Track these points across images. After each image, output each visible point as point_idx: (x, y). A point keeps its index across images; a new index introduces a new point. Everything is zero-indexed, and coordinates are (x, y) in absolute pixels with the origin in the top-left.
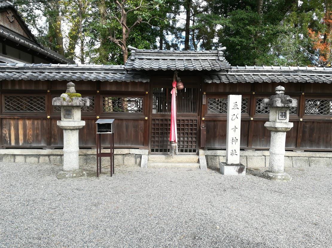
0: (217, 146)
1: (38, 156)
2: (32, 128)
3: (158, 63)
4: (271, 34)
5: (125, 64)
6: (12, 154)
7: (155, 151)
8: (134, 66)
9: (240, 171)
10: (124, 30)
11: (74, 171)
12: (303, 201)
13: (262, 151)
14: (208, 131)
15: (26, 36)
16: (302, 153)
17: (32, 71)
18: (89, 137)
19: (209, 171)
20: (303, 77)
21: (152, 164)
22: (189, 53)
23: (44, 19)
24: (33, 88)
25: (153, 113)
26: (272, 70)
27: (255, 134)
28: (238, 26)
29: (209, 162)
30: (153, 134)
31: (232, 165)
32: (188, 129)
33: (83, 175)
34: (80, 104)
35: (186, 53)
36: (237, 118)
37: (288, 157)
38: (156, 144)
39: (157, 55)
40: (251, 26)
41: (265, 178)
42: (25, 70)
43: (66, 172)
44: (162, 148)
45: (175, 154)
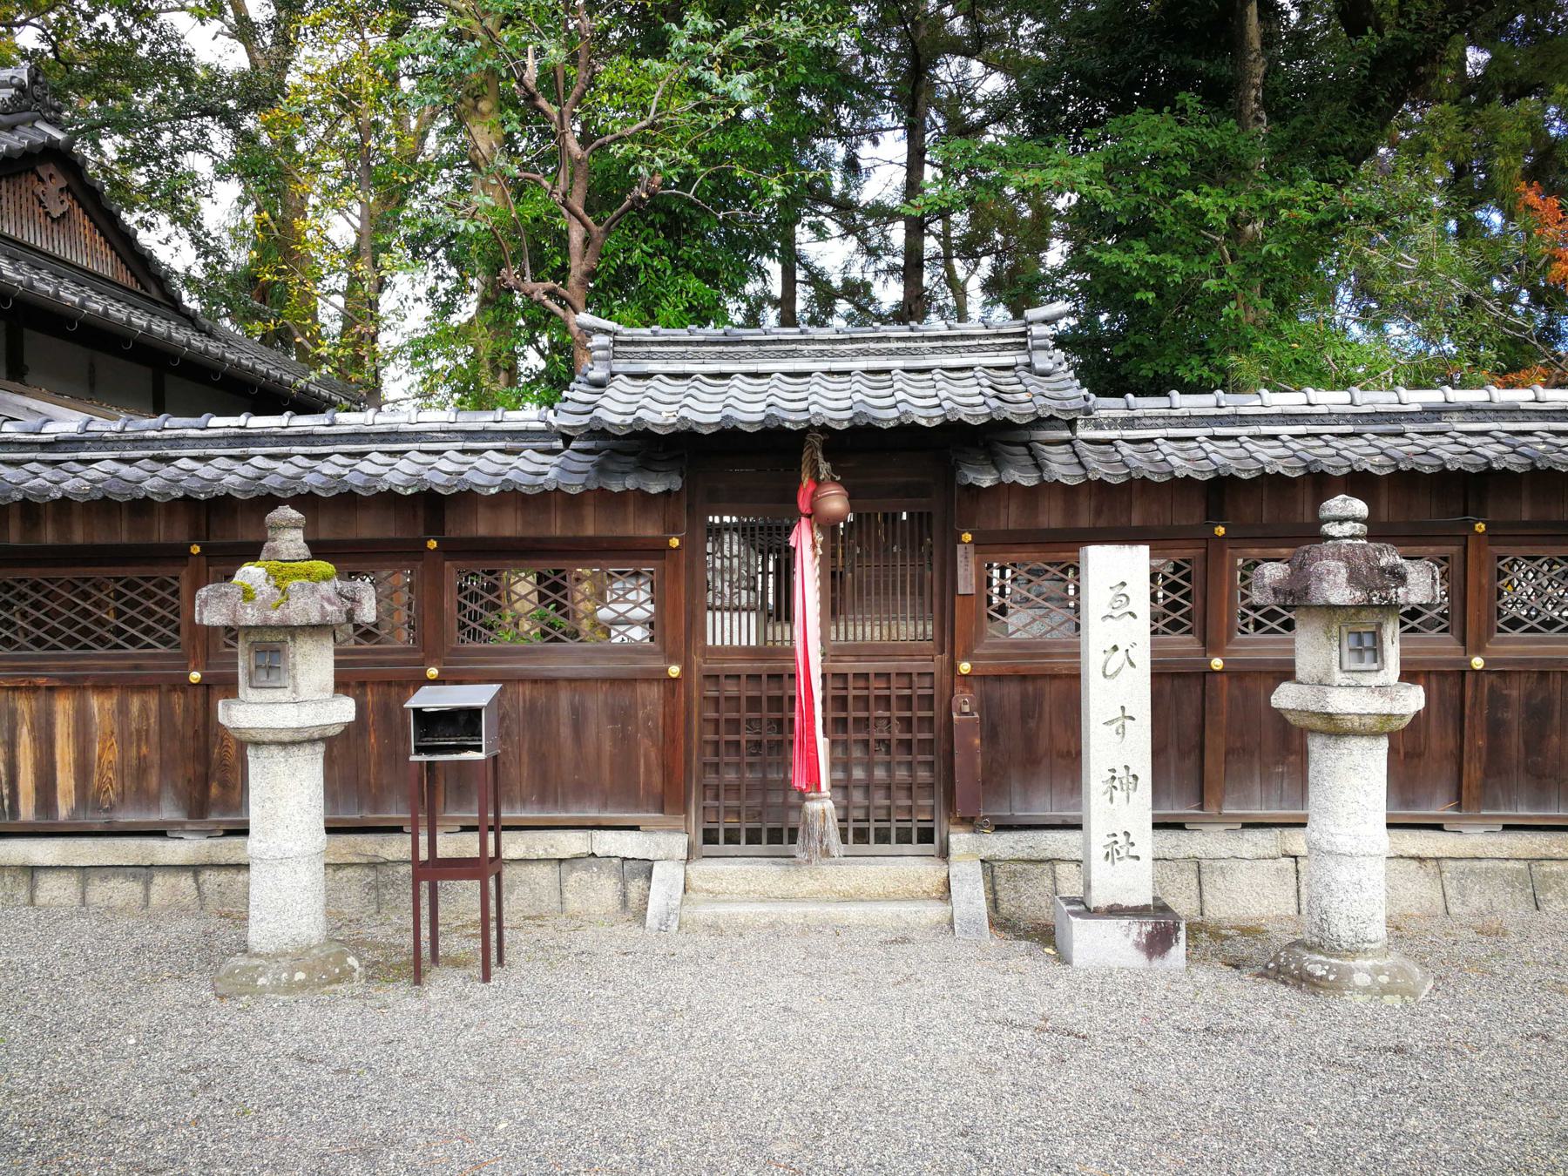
0: (1043, 808)
1: (144, 871)
2: (116, 731)
3: (722, 397)
4: (1309, 227)
5: (557, 405)
6: (19, 862)
7: (721, 838)
8: (598, 412)
9: (1158, 943)
10: (576, 236)
11: (299, 956)
12: (1476, 1124)
13: (1277, 831)
14: (991, 733)
15: (125, 278)
16: (1493, 838)
17: (116, 454)
18: (392, 771)
19: (992, 942)
20: (1470, 441)
21: (705, 912)
22: (879, 340)
23: (230, 190)
24: (123, 534)
25: (710, 642)
26: (1308, 410)
27: (1223, 744)
28: (1137, 190)
29: (1001, 894)
30: (709, 750)
31: (1115, 911)
32: (889, 720)
33: (345, 975)
34: (324, 614)
35: (864, 340)
36: (1132, 664)
37: (1420, 859)
38: (728, 803)
39: (720, 356)
40: (1206, 188)
41: (1284, 983)
42: (88, 449)
43: (257, 962)
44: (758, 825)
45: (827, 853)
